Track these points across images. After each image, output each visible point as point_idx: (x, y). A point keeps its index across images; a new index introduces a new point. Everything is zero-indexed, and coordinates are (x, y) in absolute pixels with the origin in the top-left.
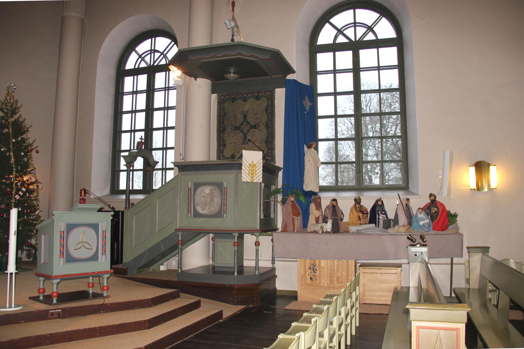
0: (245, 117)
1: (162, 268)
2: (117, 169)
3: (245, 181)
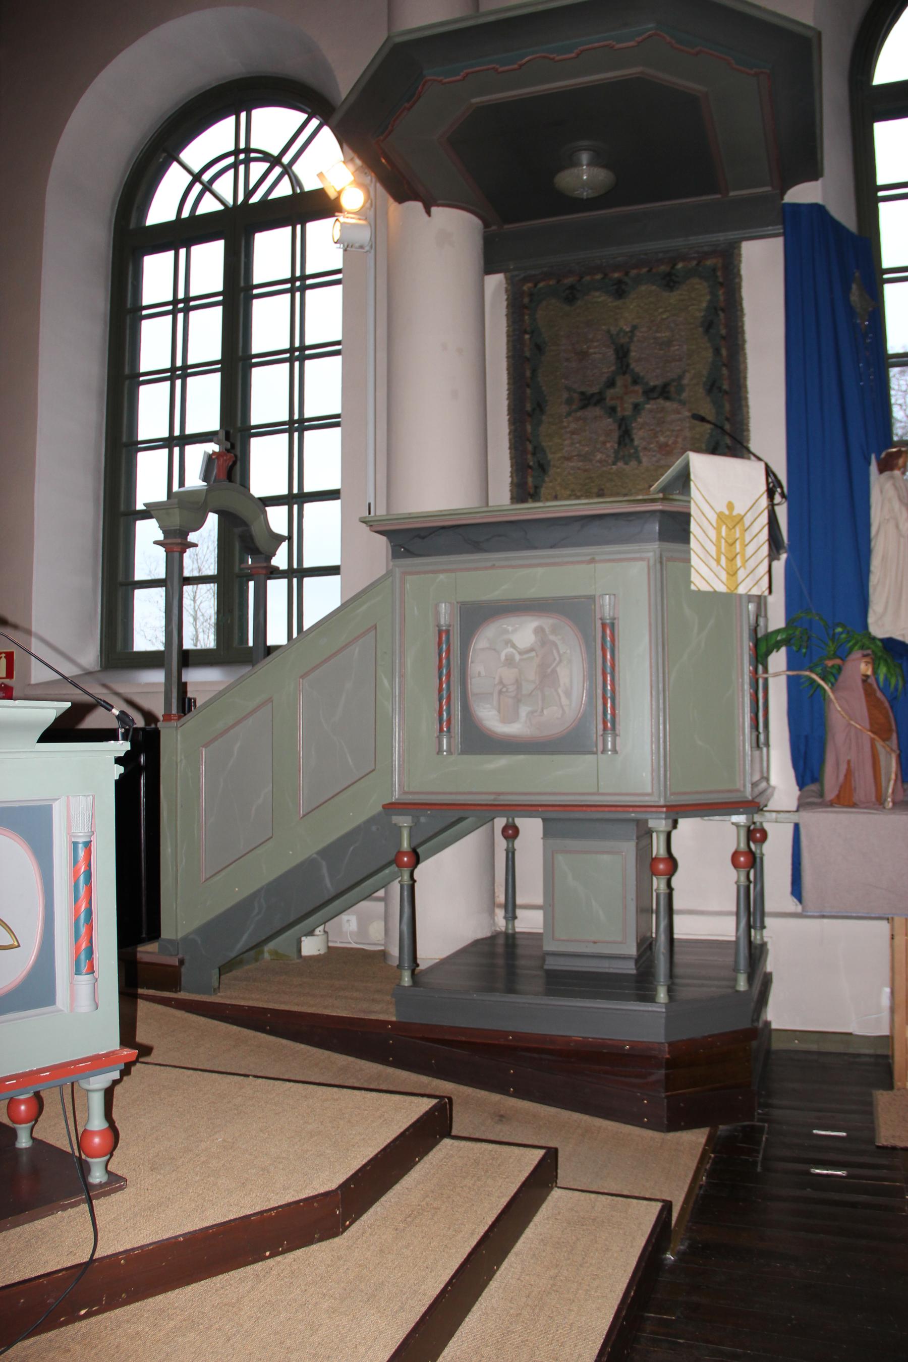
0: (622, 354)
1: (311, 946)
2: (121, 578)
3: (704, 587)
